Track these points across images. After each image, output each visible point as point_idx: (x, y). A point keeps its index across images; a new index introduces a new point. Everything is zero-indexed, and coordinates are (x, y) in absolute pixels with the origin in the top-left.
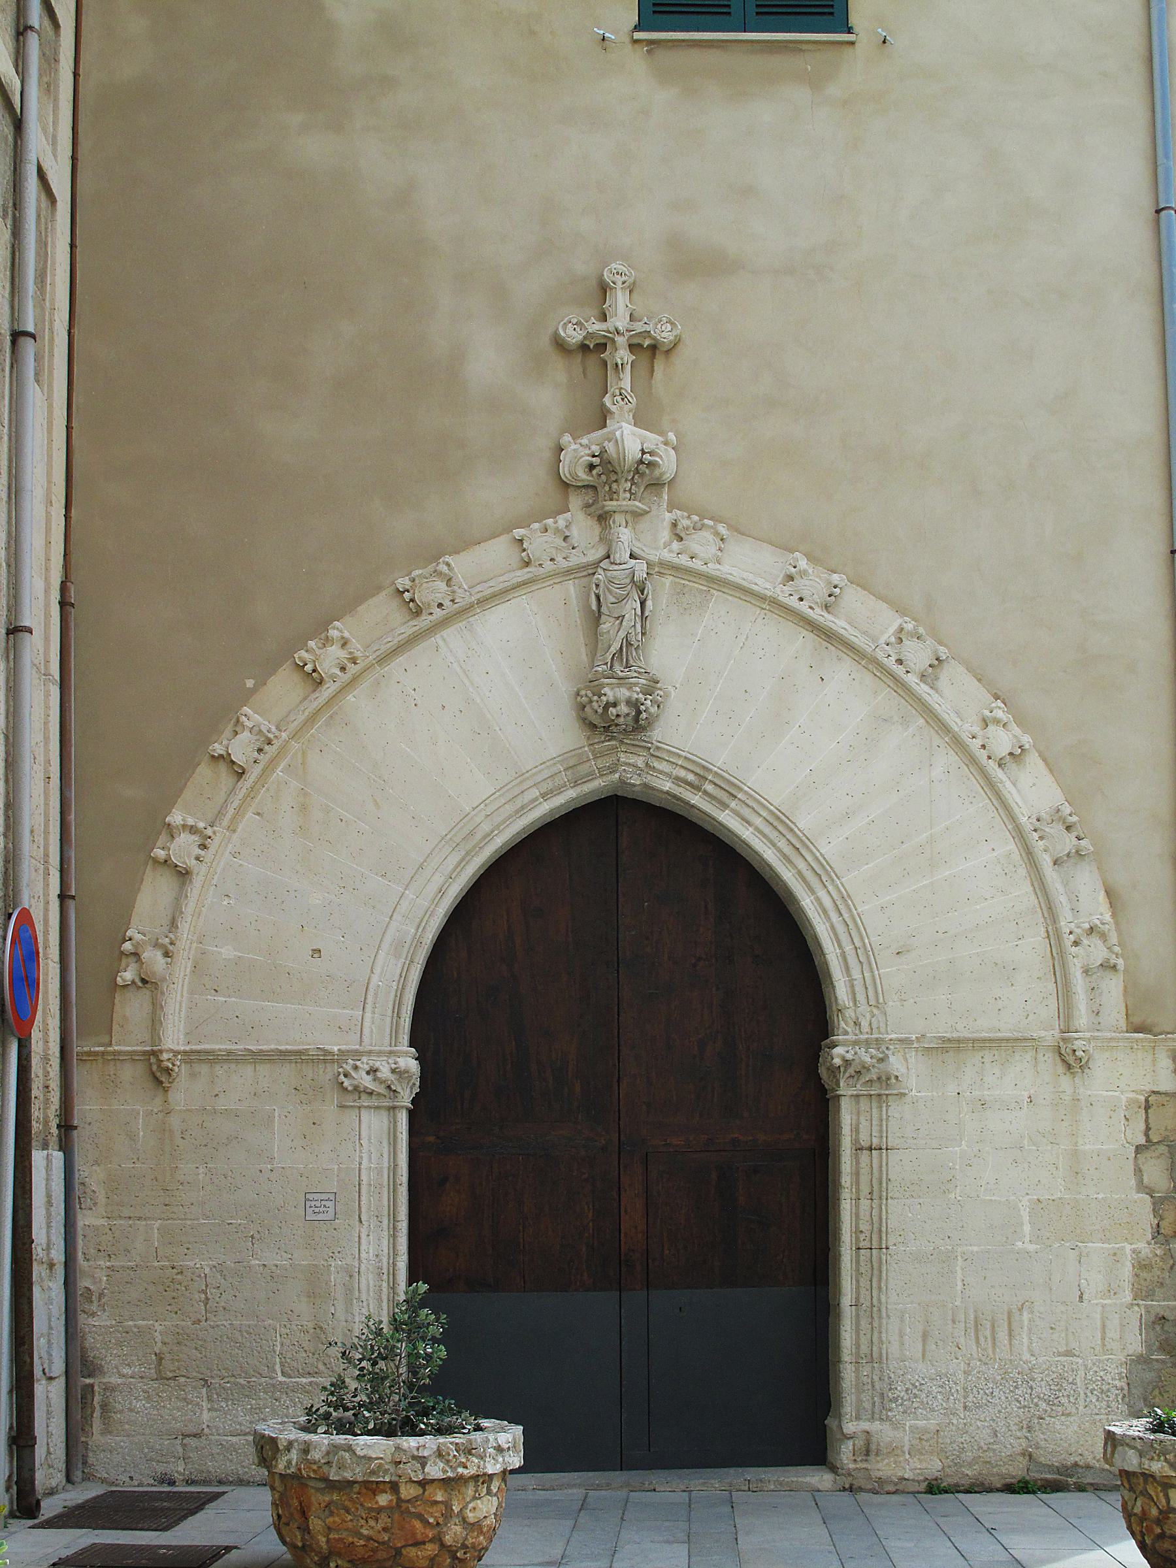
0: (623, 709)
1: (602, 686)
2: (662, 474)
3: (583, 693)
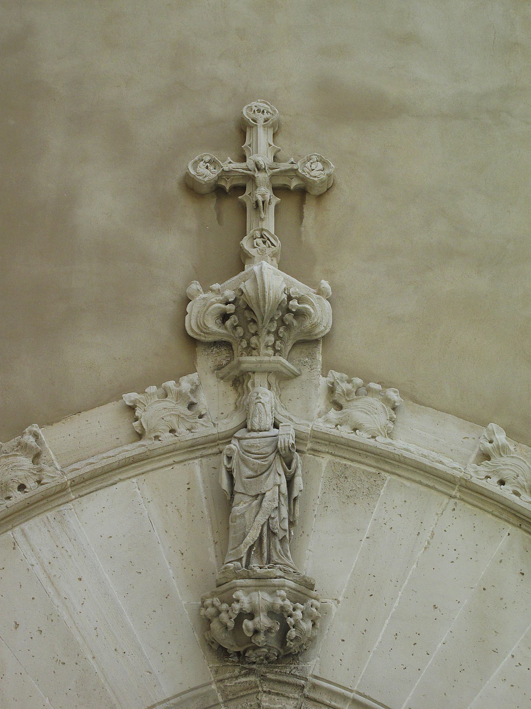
0: (263, 620)
1: (234, 589)
2: (315, 326)
3: (208, 602)
